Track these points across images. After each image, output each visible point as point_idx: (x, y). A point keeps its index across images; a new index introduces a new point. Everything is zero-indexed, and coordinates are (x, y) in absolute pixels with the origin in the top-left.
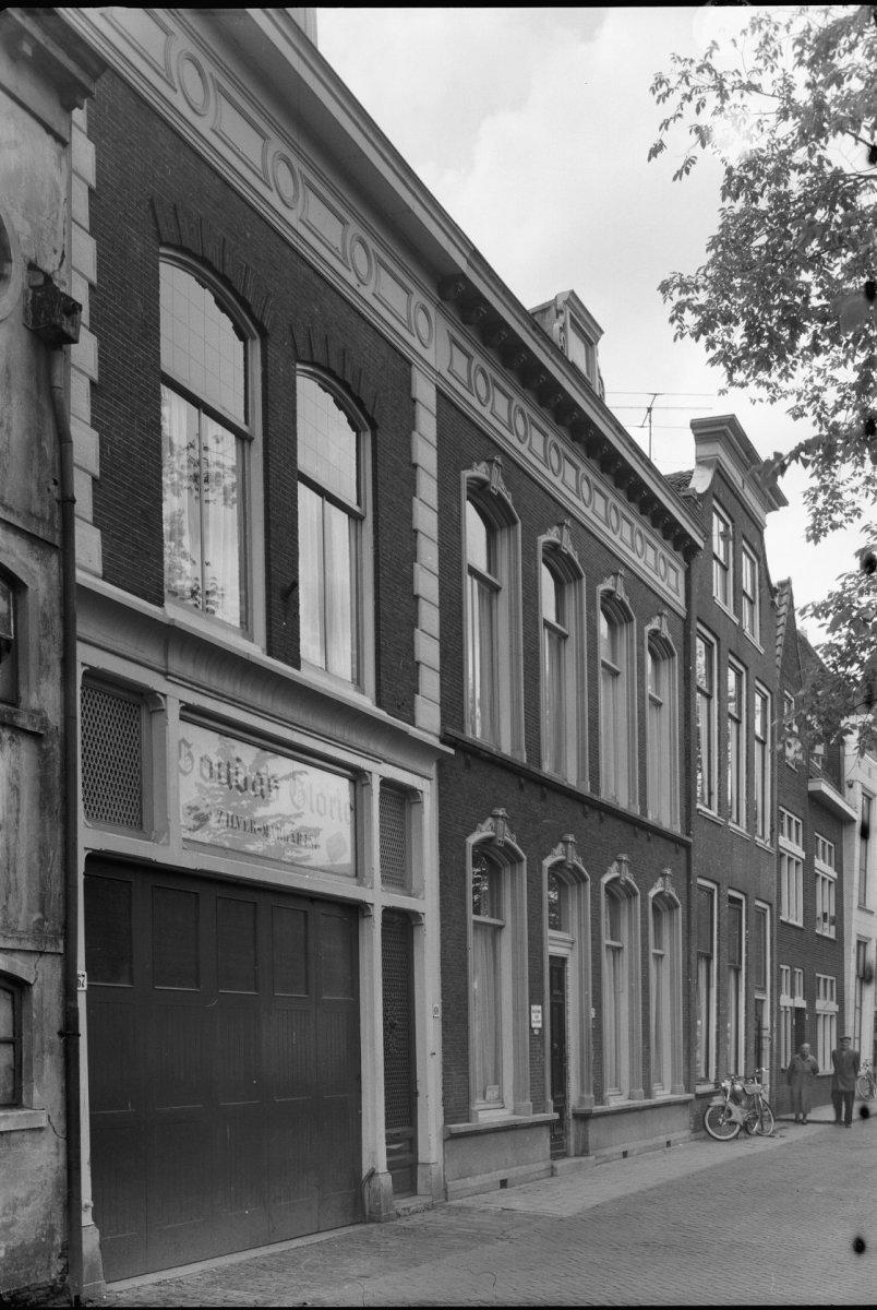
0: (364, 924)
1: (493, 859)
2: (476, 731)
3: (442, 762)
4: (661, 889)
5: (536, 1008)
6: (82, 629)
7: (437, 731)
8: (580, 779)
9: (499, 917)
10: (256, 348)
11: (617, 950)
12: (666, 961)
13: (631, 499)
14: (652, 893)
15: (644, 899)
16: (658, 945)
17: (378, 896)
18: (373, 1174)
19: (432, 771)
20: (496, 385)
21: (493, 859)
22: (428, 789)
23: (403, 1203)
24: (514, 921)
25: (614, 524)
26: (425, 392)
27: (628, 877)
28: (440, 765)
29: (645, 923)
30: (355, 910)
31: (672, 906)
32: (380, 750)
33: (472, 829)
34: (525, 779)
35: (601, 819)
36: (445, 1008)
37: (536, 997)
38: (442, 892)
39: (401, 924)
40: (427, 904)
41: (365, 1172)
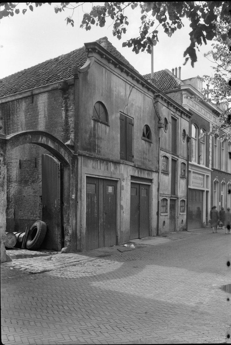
0: (204, 193)
1: (216, 183)
2: (214, 168)
3: (212, 172)
4: (223, 181)
5: (220, 202)
6: (189, 167)
7: (211, 168)
8: (225, 170)
9: (215, 190)
10: (197, 130)
11: (215, 192)
12: (216, 192)
13: (215, 114)
14: (221, 182)
15: (220, 183)
16: (215, 189)
17: (206, 190)
18: (204, 222)
19: (210, 173)
20: (208, 112)
21: (216, 183)
22: (210, 175)
23: (207, 226)
24: (217, 190)
25: (200, 110)
26: (211, 125)
27: (218, 180)
28: (211, 172)
29: (220, 187)
30: (203, 191)
31: (218, 182)
32: (206, 172)
33: (214, 179)
34: (220, 171)
35: (221, 173)
36: (211, 202)
37: (220, 201)
38: (211, 188)
39: (207, 192)
40: (209, 190)
41: (203, 222)
